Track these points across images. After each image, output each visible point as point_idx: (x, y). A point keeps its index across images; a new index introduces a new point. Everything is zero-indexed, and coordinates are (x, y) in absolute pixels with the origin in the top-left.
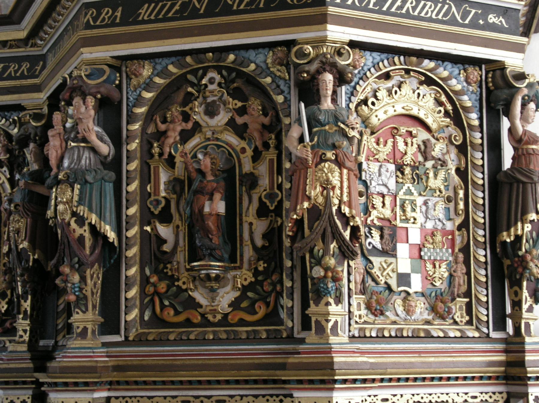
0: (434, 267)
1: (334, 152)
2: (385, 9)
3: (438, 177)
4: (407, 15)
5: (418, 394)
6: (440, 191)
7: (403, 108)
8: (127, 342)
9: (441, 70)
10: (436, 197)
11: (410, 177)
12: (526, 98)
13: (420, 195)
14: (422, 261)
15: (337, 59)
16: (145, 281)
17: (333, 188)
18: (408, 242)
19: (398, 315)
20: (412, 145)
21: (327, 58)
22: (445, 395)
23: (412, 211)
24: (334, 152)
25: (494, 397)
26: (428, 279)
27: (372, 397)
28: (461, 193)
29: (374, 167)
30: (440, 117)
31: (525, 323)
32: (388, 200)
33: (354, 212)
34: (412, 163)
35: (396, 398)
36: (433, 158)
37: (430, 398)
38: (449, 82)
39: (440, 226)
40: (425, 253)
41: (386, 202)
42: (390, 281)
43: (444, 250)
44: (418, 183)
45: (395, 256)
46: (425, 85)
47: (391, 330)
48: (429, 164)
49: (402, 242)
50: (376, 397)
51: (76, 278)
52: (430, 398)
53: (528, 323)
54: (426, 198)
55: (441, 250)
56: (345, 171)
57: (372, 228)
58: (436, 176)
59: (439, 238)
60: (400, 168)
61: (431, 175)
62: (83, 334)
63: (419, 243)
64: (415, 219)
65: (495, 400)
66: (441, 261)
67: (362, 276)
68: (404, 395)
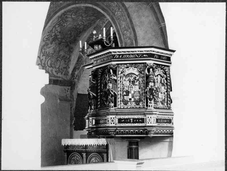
2: (115, 58)
4: (127, 58)
8: (118, 108)
16: (101, 102)
25: (144, 117)
28: (142, 85)
29: (125, 82)
47: (129, 107)
48: (136, 81)
56: (112, 84)
60: (130, 82)
61: (136, 82)
62: (112, 107)
66: (138, 96)
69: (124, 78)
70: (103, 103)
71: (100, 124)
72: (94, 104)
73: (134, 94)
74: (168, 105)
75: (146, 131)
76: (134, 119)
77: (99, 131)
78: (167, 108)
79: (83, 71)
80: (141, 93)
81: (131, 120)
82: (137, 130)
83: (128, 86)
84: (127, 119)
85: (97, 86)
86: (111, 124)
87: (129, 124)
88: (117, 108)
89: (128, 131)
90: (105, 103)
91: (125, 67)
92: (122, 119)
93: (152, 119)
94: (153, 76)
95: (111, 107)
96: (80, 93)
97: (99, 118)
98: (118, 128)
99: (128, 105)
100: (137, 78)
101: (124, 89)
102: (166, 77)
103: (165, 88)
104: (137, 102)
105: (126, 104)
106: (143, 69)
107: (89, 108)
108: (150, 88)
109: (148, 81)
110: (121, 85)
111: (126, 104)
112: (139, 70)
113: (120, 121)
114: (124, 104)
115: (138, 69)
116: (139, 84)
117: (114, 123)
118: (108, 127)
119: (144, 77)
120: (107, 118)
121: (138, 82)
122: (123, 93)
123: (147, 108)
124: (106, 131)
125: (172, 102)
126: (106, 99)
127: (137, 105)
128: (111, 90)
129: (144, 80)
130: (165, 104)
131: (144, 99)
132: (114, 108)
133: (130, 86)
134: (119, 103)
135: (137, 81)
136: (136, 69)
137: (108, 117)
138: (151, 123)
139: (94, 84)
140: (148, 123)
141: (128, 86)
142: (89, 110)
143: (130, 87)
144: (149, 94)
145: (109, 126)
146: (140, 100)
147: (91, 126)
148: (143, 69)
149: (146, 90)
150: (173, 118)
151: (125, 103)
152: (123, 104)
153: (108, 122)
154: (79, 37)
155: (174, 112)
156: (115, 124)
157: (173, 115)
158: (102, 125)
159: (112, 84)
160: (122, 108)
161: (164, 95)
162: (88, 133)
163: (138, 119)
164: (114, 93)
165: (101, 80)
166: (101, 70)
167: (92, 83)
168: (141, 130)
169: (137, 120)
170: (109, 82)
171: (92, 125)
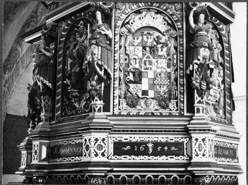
0: (160, 87)
1: (95, 40)
3: (163, 51)
5: (142, 137)
6: (165, 56)
7: (146, 24)
8: (114, 115)
9: (162, 7)
10: (162, 59)
11: (149, 51)
12: (196, 12)
13: (154, 58)
14: (155, 85)
15: (105, 6)
16: (63, 101)
17: (95, 54)
18: (147, 78)
19: (142, 107)
20: (151, 39)
21: (97, 6)
22: (156, 138)
23: (149, 65)
24: (95, 40)
25: (182, 140)
26: (157, 92)
27: (120, 138)
28: (175, 56)
30: (165, 26)
31: (197, 108)
32: (138, 61)
33: (103, 63)
34: (150, 46)
35: (132, 138)
36: (161, 43)
37: (149, 139)
38: (167, 11)
39: (164, 71)
40: (156, 82)
41: (137, 62)
42: (138, 93)
43: (166, 80)
44: (153, 54)
45: (141, 83)
46: (159, 14)
47: (143, 113)
48: (159, 46)
49: (145, 78)
50: (122, 138)
51: (39, 101)
52: (149, 139)
53: (199, 108)
54: (157, 59)
55: (164, 80)
56: (100, 48)
57: (130, 72)
58: (162, 50)
59: (163, 75)
60: (144, 48)
61: (160, 49)
62: (99, 110)
63: (153, 78)
64: (151, 68)
65: (183, 141)
66: (164, 85)
67: (124, 92)
68: (135, 138)
69: (130, 38)
70: (68, 106)
71: (59, 156)
72: (45, 106)
73: (154, 80)
74: (227, 115)
75: (161, 178)
76: (156, 144)
77: (56, 177)
78: (227, 122)
79: (18, 75)
80: (173, 76)
81: (150, 145)
82: (162, 175)
83: (141, 59)
84: (138, 144)
85: (55, 65)
86: (96, 155)
87: (142, 157)
88: (111, 113)
89: (153, 175)
90: (76, 105)
91: (133, 10)
92: (126, 144)
93: (207, 144)
94: (206, 34)
95: (97, 109)
96: (10, 114)
97: (60, 142)
98: (115, 169)
99: (138, 107)
100: (163, 41)
101: (129, 66)
102: (221, 48)
103: (219, 73)
104: (163, 103)
105: (133, 105)
106: (180, 16)
107: (31, 125)
108: (200, 63)
109: (197, 45)
110: (121, 56)
111: (133, 105)
112: (166, 20)
113: (119, 148)
114: (127, 104)
115: (164, 19)
116: (168, 55)
117: (103, 155)
118: (88, 164)
119: (182, 37)
120: (83, 141)
121: (165, 49)
122: (126, 76)
123: (193, 116)
124: (76, 176)
125: (234, 109)
126: (79, 92)
127: (163, 107)
128: (98, 64)
129: (182, 45)
130: (221, 112)
131: (180, 93)
132: (102, 114)
133: (145, 59)
134: (116, 101)
135: (162, 47)
136: (160, 17)
137: (87, 137)
138: (204, 155)
139: (49, 58)
140: (197, 155)
141: (141, 59)
142: (29, 129)
143: (145, 62)
144: (197, 77)
145: (90, 162)
146: (171, 96)
147: (35, 162)
148: (180, 16)
149: (191, 66)
150: (238, 145)
151: (130, 102)
152: (125, 103)
153: (87, 149)
154: (14, 14)
155: (239, 133)
156: (106, 156)
157: (239, 139)
158: (66, 161)
159: (102, 47)
160: (125, 114)
161: (219, 90)
162: (24, 180)
163: (167, 144)
164: (106, 71)
165: (66, 48)
166: (68, 25)
167: (44, 55)
168: (175, 175)
169: (166, 148)
170: (94, 42)
171: (40, 160)
